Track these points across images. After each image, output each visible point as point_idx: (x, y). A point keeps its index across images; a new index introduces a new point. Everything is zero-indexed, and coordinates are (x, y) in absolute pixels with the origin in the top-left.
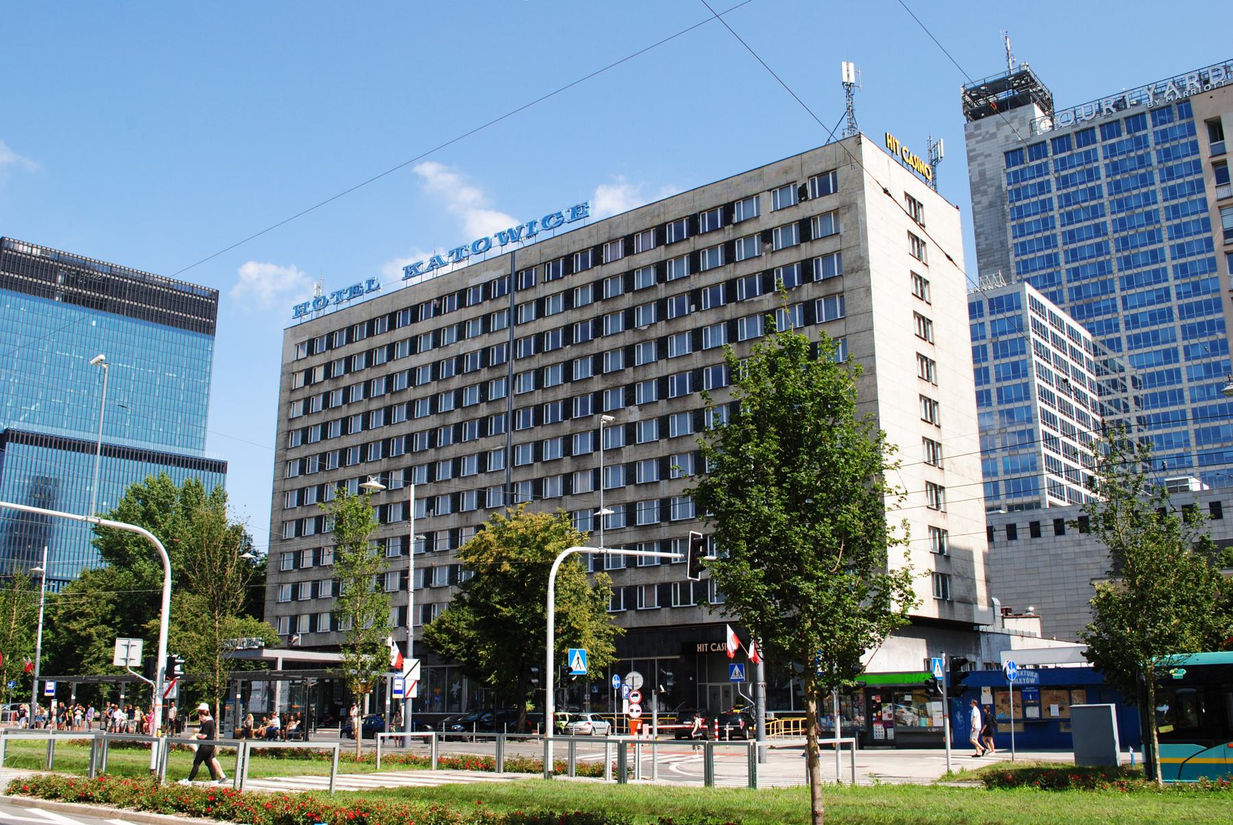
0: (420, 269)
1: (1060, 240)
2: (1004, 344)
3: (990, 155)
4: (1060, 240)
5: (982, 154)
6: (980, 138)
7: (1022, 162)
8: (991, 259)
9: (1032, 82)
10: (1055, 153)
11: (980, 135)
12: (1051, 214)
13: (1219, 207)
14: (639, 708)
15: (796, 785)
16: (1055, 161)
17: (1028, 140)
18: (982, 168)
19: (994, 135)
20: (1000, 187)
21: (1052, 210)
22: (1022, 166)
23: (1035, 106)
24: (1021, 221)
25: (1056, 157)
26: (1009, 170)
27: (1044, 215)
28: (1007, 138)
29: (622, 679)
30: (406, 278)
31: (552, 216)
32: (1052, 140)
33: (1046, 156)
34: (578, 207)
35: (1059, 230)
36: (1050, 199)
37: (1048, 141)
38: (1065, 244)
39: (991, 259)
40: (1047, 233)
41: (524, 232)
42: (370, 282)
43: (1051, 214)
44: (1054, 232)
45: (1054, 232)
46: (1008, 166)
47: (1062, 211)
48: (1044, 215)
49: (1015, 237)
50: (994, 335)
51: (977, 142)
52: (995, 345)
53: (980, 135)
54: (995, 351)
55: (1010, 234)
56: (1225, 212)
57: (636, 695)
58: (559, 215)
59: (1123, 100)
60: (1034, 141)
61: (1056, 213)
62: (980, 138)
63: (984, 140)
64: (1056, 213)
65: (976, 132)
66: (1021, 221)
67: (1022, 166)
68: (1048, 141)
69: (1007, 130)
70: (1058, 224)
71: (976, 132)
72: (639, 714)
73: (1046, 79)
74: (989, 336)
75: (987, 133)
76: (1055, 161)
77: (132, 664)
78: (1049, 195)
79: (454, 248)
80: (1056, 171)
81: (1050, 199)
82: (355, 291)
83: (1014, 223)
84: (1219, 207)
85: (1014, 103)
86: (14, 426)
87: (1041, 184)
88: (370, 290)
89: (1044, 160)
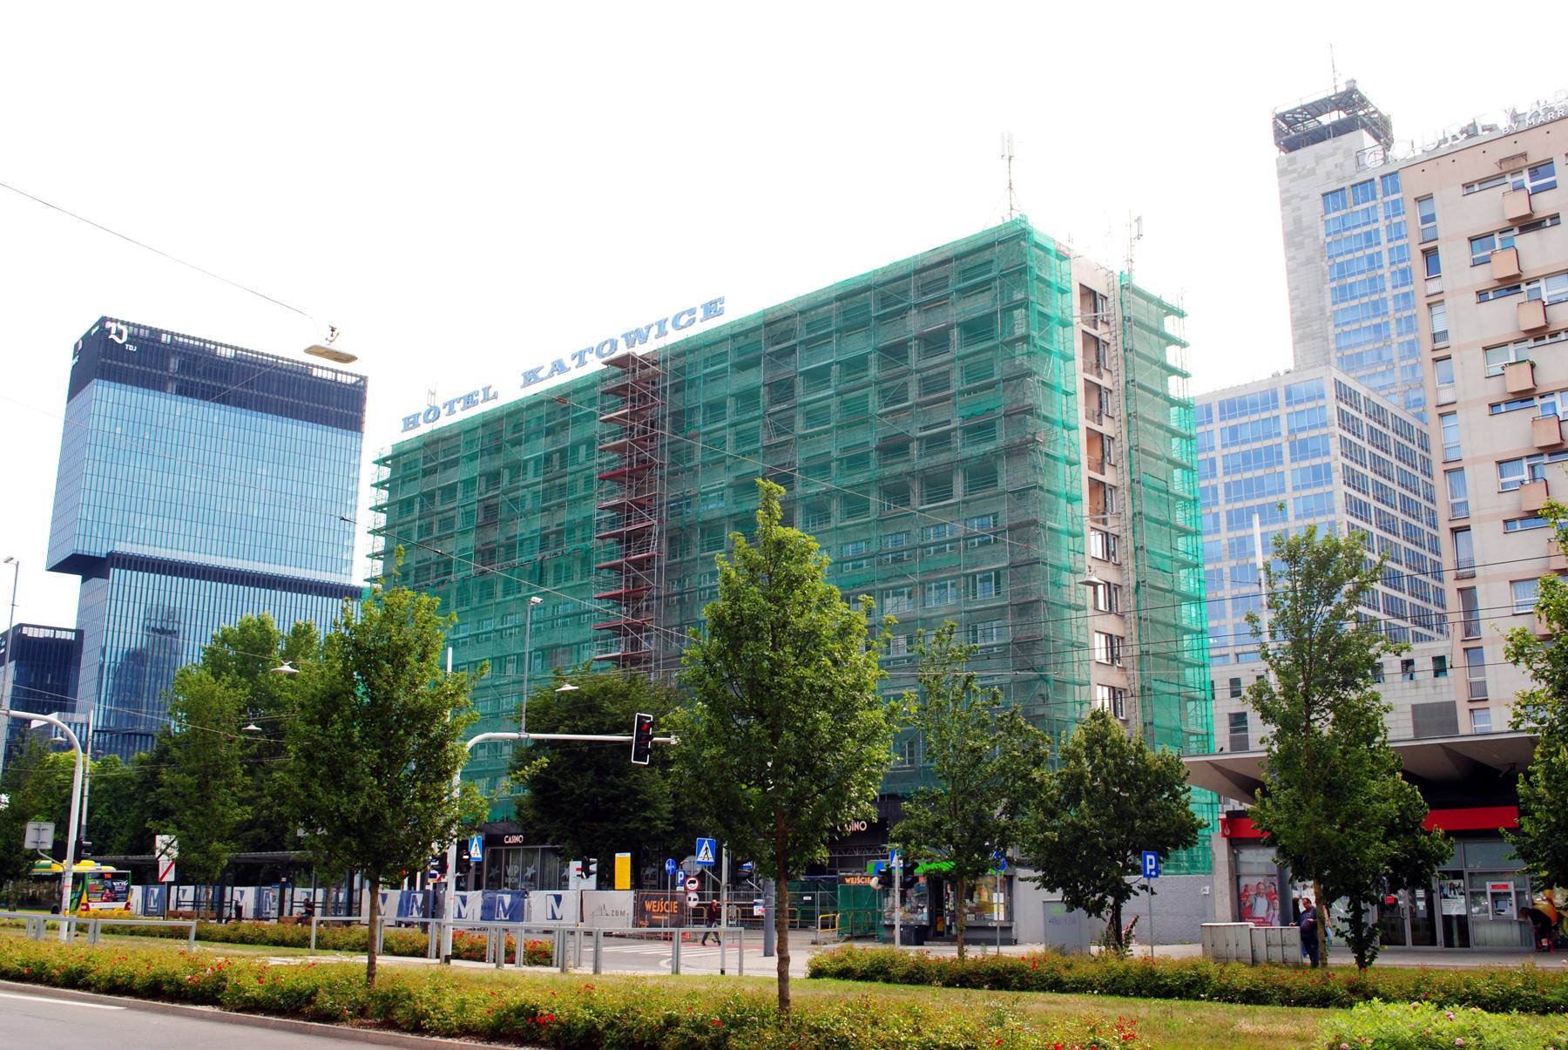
0: (541, 374)
1: (1391, 305)
2: (1304, 443)
3: (1307, 197)
4: (1391, 305)
5: (1296, 196)
6: (1296, 175)
7: (1345, 207)
8: (1308, 330)
9: (1363, 102)
10: (1386, 194)
11: (1294, 171)
12: (1380, 272)
13: (1429, 305)
14: (696, 896)
15: (1447, 1010)
16: (1386, 204)
17: (1352, 178)
18: (1298, 213)
19: (1312, 172)
20: (1318, 237)
21: (1381, 267)
22: (1344, 212)
23: (1364, 132)
24: (1343, 282)
25: (1387, 199)
26: (1328, 217)
27: (1372, 274)
28: (1328, 175)
29: (678, 865)
30: (406, 429)
31: (683, 313)
32: (1382, 177)
33: (1374, 198)
34: (711, 303)
35: (1389, 293)
36: (1379, 253)
37: (1377, 179)
38: (1397, 310)
39: (1308, 330)
40: (1375, 297)
41: (654, 330)
42: (486, 390)
43: (1380, 272)
44: (1384, 295)
45: (1384, 295)
46: (1327, 212)
47: (1394, 268)
48: (1372, 274)
49: (1334, 303)
50: (1291, 431)
51: (1292, 181)
52: (1292, 444)
53: (1294, 171)
54: (1292, 452)
55: (1328, 299)
56: (1436, 310)
57: (694, 882)
58: (692, 312)
59: (1474, 125)
60: (1389, 169)
61: (1386, 271)
62: (1296, 175)
63: (1300, 177)
64: (1386, 271)
65: (1290, 168)
66: (1343, 282)
67: (1344, 212)
68: (1377, 179)
69: (1329, 164)
70: (1388, 285)
71: (1290, 168)
72: (696, 903)
73: (1380, 100)
74: (1285, 433)
75: (1304, 168)
76: (1386, 204)
77: (43, 847)
78: (1377, 249)
79: (446, 401)
80: (1387, 218)
81: (1379, 253)
82: (469, 401)
83: (1334, 284)
84: (1429, 305)
85: (1340, 129)
86: (122, 548)
87: (1368, 234)
88: (486, 399)
89: (1372, 203)
